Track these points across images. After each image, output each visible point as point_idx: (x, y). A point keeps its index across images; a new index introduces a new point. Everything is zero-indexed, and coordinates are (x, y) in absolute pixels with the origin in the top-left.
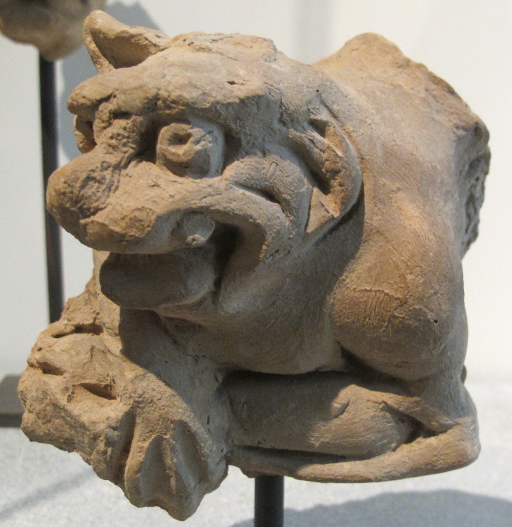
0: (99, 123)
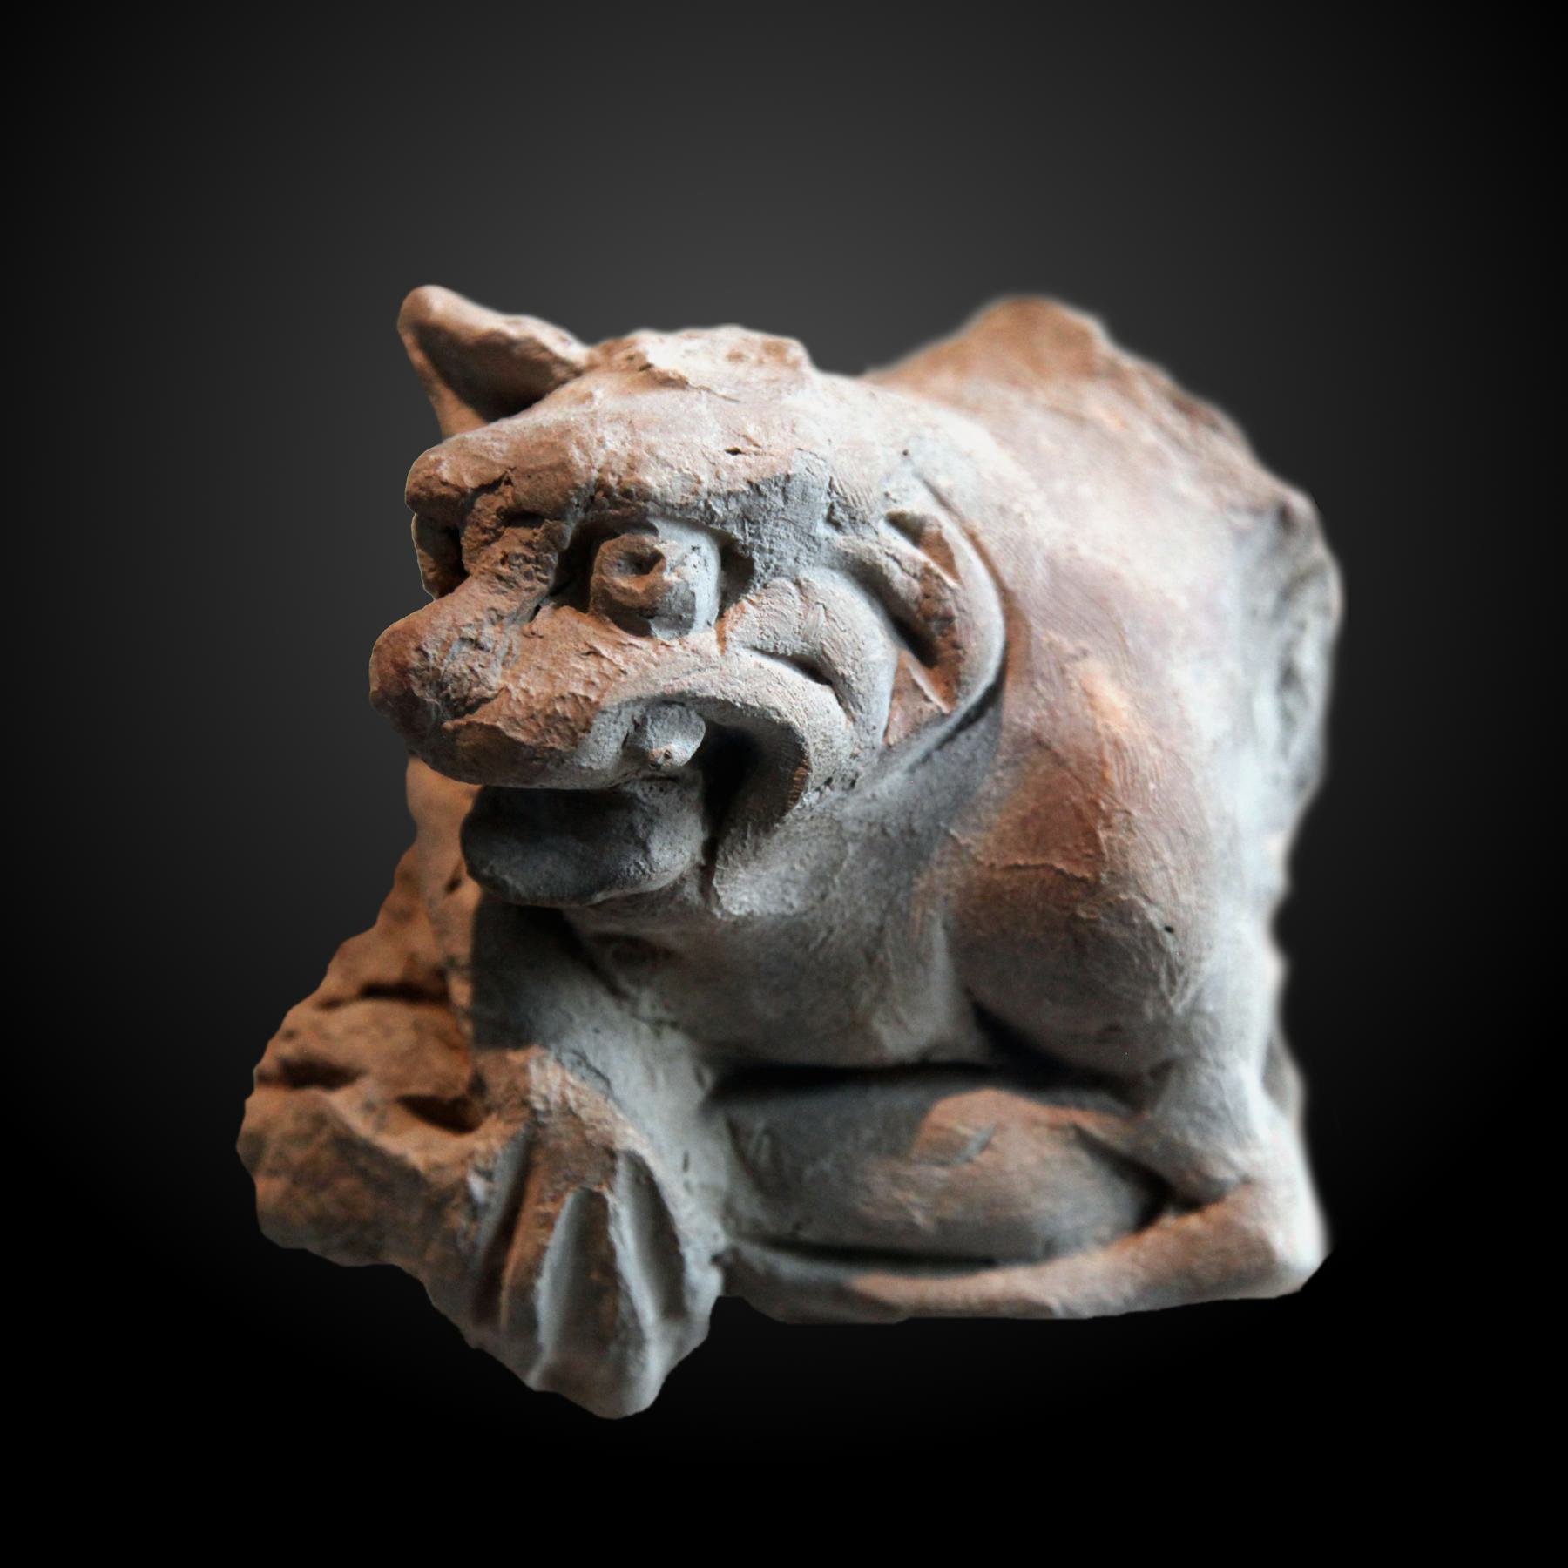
0: (475, 533)
